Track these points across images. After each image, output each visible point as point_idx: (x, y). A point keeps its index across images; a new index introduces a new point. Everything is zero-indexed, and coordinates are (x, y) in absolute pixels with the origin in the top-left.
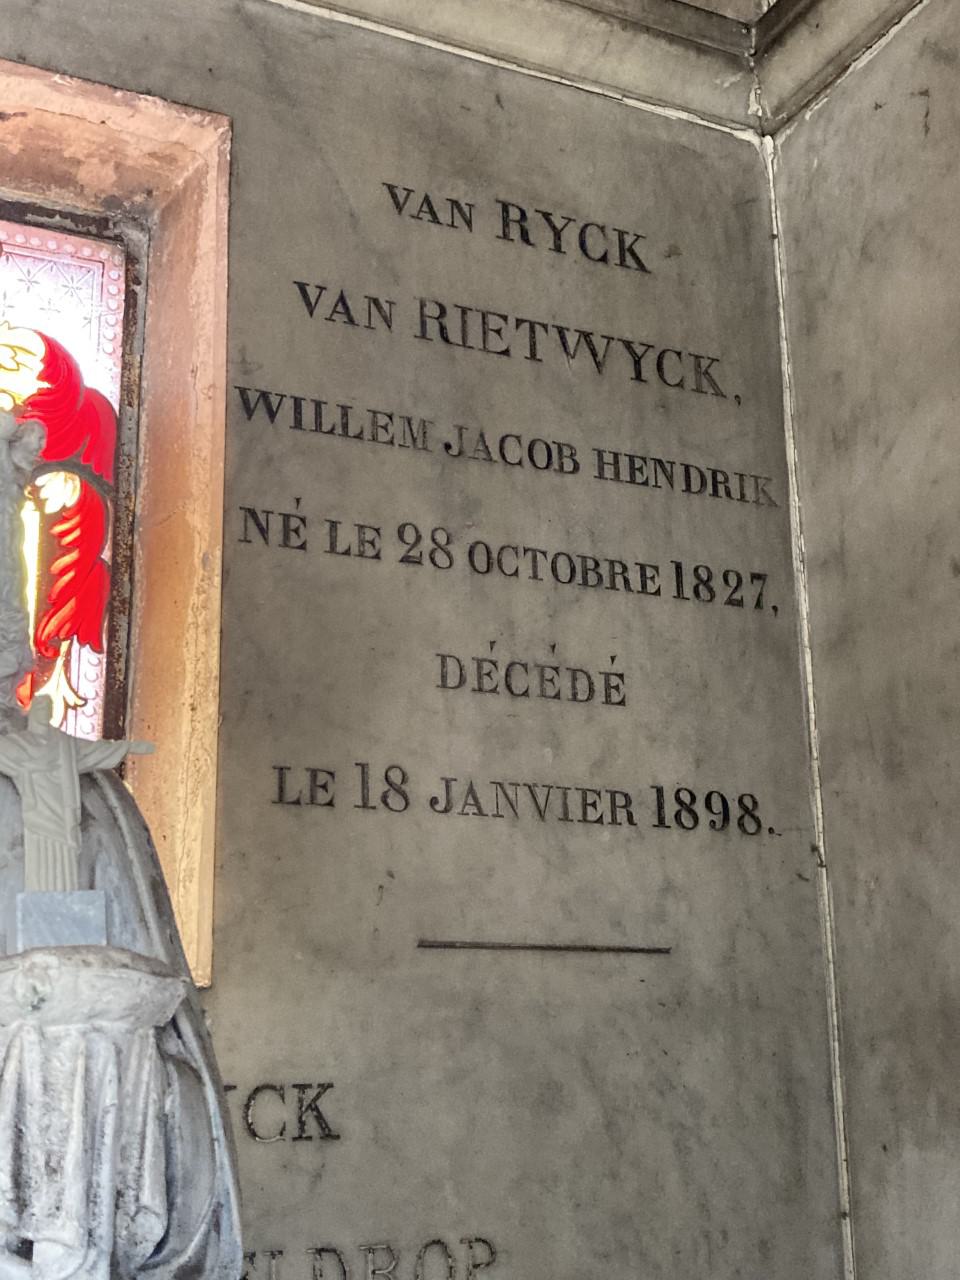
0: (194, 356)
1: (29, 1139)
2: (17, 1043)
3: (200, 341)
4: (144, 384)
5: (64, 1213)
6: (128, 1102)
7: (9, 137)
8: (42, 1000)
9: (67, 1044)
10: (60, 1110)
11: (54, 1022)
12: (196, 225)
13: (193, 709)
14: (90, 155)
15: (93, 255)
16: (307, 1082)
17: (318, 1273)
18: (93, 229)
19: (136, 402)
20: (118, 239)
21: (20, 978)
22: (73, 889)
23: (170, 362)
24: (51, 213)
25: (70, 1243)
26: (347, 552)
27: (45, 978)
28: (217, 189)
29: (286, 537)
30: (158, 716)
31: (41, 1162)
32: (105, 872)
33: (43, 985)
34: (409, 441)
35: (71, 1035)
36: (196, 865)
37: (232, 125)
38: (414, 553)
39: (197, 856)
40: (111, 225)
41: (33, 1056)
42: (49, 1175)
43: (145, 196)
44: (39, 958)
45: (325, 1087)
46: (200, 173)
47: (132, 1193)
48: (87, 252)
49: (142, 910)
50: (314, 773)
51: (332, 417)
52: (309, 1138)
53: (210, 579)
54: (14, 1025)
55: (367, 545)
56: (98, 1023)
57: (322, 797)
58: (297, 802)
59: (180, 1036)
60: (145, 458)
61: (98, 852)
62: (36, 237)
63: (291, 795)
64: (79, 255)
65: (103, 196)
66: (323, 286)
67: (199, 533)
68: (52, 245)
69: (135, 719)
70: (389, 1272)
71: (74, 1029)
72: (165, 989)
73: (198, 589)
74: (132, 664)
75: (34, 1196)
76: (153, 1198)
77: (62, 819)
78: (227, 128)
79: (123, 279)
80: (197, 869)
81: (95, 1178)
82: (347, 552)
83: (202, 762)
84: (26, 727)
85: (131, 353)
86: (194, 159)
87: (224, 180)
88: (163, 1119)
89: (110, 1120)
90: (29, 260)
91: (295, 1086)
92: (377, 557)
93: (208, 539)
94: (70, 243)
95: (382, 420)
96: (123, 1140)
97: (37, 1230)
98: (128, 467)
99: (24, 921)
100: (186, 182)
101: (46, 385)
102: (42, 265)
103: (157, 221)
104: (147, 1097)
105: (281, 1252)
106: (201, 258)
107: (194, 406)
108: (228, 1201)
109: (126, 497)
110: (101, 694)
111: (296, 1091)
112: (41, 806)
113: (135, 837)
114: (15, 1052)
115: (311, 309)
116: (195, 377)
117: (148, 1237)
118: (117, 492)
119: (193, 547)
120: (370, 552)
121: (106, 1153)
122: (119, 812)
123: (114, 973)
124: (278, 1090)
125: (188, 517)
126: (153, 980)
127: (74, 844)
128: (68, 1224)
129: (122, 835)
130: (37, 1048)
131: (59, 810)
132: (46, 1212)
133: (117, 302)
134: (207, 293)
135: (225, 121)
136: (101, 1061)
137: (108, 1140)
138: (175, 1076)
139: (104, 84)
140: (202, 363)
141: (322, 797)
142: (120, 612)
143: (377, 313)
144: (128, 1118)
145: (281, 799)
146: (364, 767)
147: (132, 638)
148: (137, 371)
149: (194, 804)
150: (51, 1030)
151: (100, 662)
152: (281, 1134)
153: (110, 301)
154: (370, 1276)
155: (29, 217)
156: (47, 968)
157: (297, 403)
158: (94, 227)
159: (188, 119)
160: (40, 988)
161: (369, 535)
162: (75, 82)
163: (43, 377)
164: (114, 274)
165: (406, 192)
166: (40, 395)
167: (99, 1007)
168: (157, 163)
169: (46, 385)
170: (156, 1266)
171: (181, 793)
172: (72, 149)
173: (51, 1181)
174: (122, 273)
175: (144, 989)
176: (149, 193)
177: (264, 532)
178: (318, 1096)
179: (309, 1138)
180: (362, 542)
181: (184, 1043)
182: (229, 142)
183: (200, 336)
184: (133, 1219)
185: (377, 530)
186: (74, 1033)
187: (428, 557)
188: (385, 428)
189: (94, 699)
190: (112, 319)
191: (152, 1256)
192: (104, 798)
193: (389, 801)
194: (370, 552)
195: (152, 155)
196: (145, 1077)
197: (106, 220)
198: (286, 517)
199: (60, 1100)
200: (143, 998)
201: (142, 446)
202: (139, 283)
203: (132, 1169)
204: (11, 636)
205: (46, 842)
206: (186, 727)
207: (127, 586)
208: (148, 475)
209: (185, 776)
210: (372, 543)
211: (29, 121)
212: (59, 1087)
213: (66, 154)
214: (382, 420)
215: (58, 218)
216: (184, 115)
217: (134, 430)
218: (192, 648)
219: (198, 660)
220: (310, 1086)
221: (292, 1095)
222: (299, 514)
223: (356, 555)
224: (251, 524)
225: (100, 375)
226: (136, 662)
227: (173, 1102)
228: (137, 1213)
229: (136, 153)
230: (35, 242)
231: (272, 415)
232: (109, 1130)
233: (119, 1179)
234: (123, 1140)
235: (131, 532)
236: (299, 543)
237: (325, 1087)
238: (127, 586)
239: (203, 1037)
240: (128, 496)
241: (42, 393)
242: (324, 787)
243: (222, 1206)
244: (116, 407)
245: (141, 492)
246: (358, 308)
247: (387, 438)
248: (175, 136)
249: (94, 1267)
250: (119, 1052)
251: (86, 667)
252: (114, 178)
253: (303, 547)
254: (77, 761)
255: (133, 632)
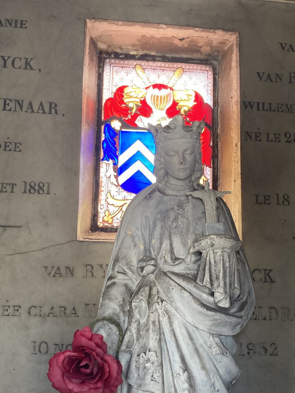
0: (232, 93)
1: (212, 272)
2: (209, 253)
3: (233, 90)
4: (219, 100)
5: (220, 287)
6: (231, 266)
7: (185, 43)
8: (213, 244)
9: (218, 254)
10: (218, 267)
11: (216, 249)
12: (231, 59)
13: (235, 181)
14: (204, 45)
15: (205, 69)
16: (266, 269)
17: (271, 313)
18: (205, 62)
19: (217, 105)
20: (211, 64)
21: (209, 240)
22: (216, 223)
23: (225, 95)
24: (195, 60)
25: (222, 293)
26: (271, 141)
27: (214, 240)
28: (236, 50)
29: (256, 138)
30: (226, 183)
31: (215, 276)
32: (221, 219)
33: (213, 241)
34: (287, 111)
35: (219, 252)
36: (237, 218)
37: (239, 34)
38: (290, 140)
39: (237, 216)
40: (209, 60)
41: (212, 256)
42: (217, 279)
43: (217, 53)
44: (212, 236)
45: (271, 270)
46: (232, 46)
47: (233, 285)
48: (203, 68)
49: (230, 228)
50: (265, 196)
51: (267, 106)
52: (267, 282)
53: (238, 150)
54: (208, 250)
55: (277, 139)
56: (225, 250)
57: (267, 202)
58: (261, 203)
59: (239, 254)
60: (219, 119)
61: (220, 215)
62: (191, 66)
63: (259, 202)
64: (202, 69)
65: (207, 54)
66: (264, 72)
67: (234, 138)
68: (195, 68)
69: (220, 184)
70: (288, 314)
71: (220, 251)
72: (237, 243)
73: (235, 152)
74: (219, 170)
75: (214, 283)
76: (237, 286)
77: (213, 208)
78: (238, 34)
79: (212, 74)
80: (238, 219)
81: (226, 281)
82: (271, 141)
83: (237, 194)
84: (204, 189)
85: (215, 93)
86: (230, 42)
87: (238, 48)
88: (238, 270)
89: (228, 269)
90: (190, 72)
91: (263, 270)
92: (280, 141)
93: (237, 140)
94: (199, 67)
95: (280, 106)
96: (231, 274)
97: (215, 290)
98: (216, 122)
99: (207, 229)
100: (227, 48)
101: (195, 103)
102: (193, 73)
103: (221, 58)
104: (235, 266)
105: (262, 307)
106: (233, 68)
107: (232, 106)
108: (252, 290)
109: (215, 130)
110: (212, 178)
111: (264, 271)
112: (209, 205)
113: (227, 212)
114: (208, 255)
115: (261, 79)
116: (232, 99)
117: (237, 294)
118: (213, 128)
119: (233, 142)
120: (278, 140)
121: (228, 276)
122: (223, 206)
123: (227, 240)
124: (260, 270)
125: (232, 134)
126: (235, 241)
127: (216, 213)
128: (221, 289)
129: (224, 211)
130: (213, 254)
131: (212, 206)
132: (216, 286)
133: (211, 80)
134: (234, 78)
135: (238, 33)
136: (226, 258)
137: (228, 273)
138: (240, 262)
139: (208, 28)
140: (234, 95)
141: (267, 202)
142: (215, 158)
143: (278, 78)
144: (231, 269)
145: (257, 203)
146: (278, 195)
147: (218, 164)
148: (217, 97)
149: (236, 203)
150: (215, 251)
151: (211, 170)
152: (261, 280)
153: (210, 80)
154: (283, 314)
155: (190, 61)
156: (214, 238)
157: (258, 104)
158: (204, 61)
159: (228, 33)
160: (213, 242)
161: (277, 136)
162: (201, 29)
163: (195, 101)
164: (210, 73)
165: (285, 44)
166: (194, 106)
167: (225, 246)
168: (220, 45)
169: (195, 103)
170: (238, 301)
171: (233, 201)
172: (200, 44)
173: (217, 281)
174: (212, 73)
175: (233, 243)
176: (218, 52)
177: (250, 138)
178: (269, 272)
179: (267, 282)
180: (275, 138)
181: (240, 256)
182: (239, 38)
183: (233, 88)
184: (233, 290)
185: (279, 135)
186: (220, 251)
187: (293, 141)
188: (281, 108)
189: (210, 179)
190: (210, 85)
191: (237, 298)
192: (220, 203)
193: (284, 203)
194: (278, 140)
195: (219, 43)
196: (234, 261)
197: (208, 60)
198: (256, 133)
199: (218, 265)
200: (234, 245)
201: (219, 117)
202: (216, 75)
203: (233, 280)
204: (199, 169)
205: (213, 214)
206: (233, 186)
207: (216, 151)
208: (221, 123)
209: (233, 197)
210: (278, 138)
211: (190, 39)
212: (218, 262)
213: (198, 45)
214: (280, 106)
215: (196, 61)
216: (227, 33)
217: (217, 113)
218: (234, 166)
219: (235, 170)
220: (267, 270)
221: (263, 272)
222: (259, 132)
223: (274, 142)
224: (247, 135)
225: (208, 100)
226: (219, 170)
227: (240, 267)
228: (234, 289)
229: (215, 43)
230: (191, 67)
231: (252, 107)
232: (228, 271)
233: (230, 282)
234: (231, 274)
235: (217, 138)
236: (259, 140)
237: (271, 270)
238: (216, 151)
239: (244, 255)
240: (216, 129)
241: (194, 106)
242: (268, 200)
243: (250, 291)
244: (212, 107)
245: (219, 128)
246: (273, 77)
247: (281, 110)
248: (225, 38)
249: (226, 298)
250: (229, 256)
251: (208, 172)
252: (210, 49)
253: (260, 140)
254: (215, 196)
255: (218, 163)
